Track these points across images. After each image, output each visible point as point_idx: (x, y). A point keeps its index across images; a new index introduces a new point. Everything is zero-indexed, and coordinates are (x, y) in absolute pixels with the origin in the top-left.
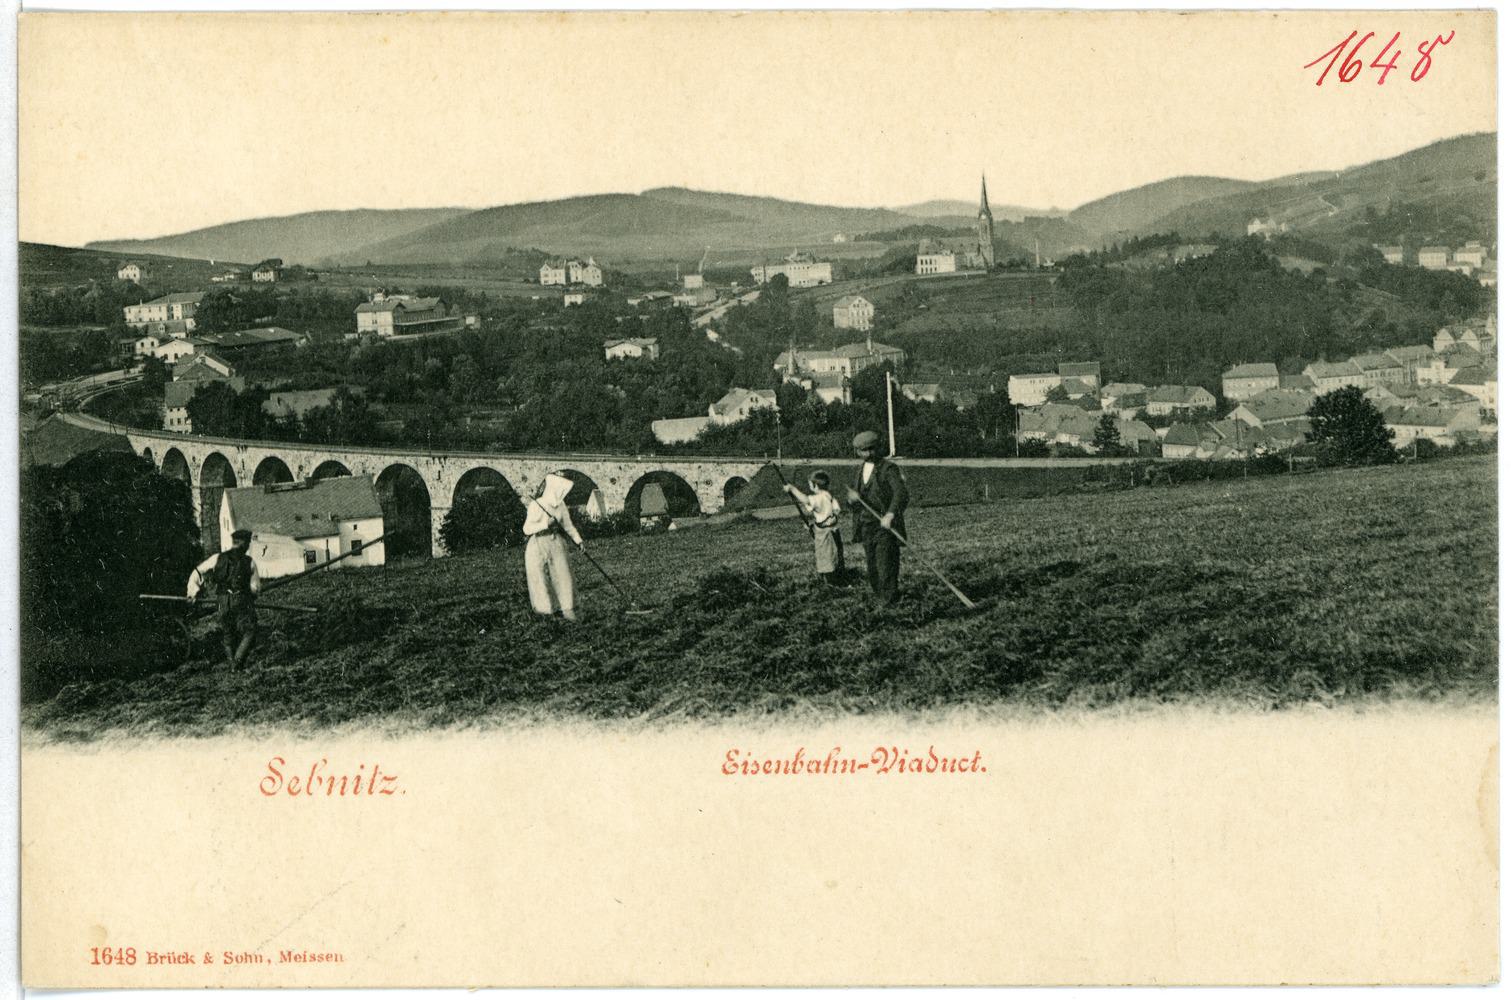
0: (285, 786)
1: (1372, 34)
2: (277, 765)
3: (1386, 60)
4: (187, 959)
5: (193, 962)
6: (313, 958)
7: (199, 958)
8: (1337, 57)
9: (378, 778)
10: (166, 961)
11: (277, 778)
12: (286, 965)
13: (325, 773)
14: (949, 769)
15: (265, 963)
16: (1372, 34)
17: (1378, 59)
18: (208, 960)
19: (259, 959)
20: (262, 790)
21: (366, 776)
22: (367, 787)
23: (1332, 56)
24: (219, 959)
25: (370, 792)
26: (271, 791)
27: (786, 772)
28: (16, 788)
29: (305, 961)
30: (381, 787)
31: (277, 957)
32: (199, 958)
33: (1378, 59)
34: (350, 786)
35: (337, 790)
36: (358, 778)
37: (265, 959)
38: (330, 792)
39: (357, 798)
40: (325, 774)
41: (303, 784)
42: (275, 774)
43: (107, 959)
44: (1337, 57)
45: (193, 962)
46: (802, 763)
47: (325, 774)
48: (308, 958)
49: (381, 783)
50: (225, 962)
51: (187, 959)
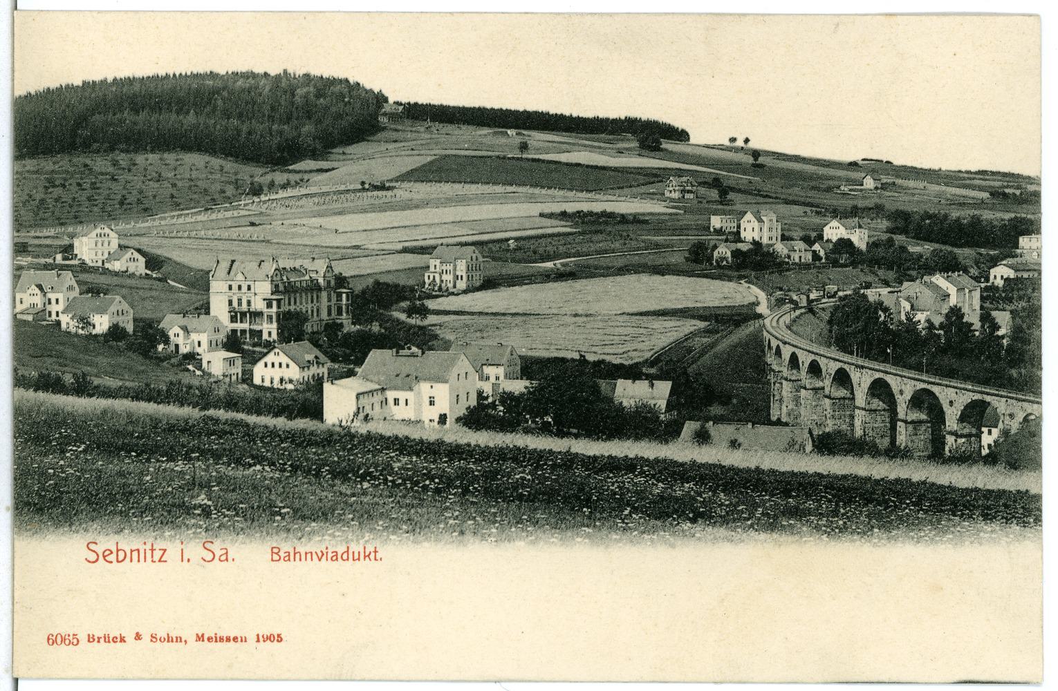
5: (125, 641)
7: (130, 638)
18: (138, 637)
19: (179, 639)
32: (130, 638)
39: (295, 563)
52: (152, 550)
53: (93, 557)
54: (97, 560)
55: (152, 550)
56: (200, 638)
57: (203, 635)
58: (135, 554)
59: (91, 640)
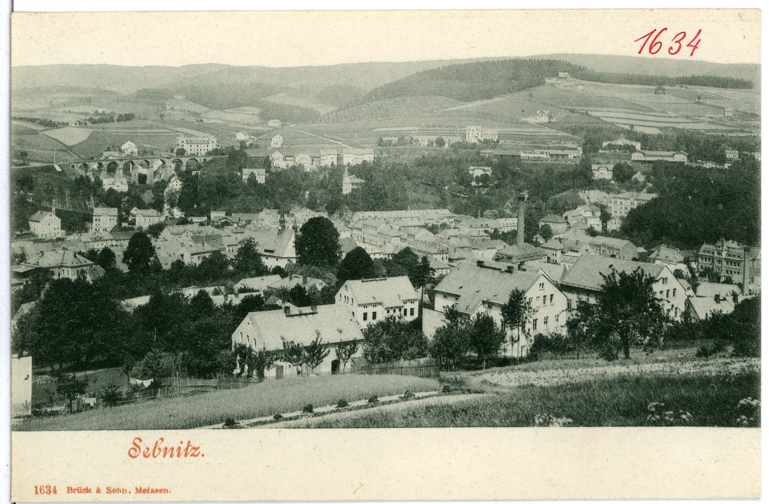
1: (666, 29)
2: (137, 442)
3: (694, 44)
4: (87, 490)
6: (152, 491)
7: (94, 490)
8: (648, 39)
9: (190, 448)
10: (76, 491)
11: (138, 449)
12: (139, 494)
13: (162, 446)
14: (175, 449)
15: (128, 493)
16: (666, 29)
17: (691, 42)
18: (98, 491)
20: (130, 455)
21: (184, 446)
22: (184, 453)
23: (647, 37)
24: (104, 490)
25: (186, 455)
26: (133, 455)
27: (172, 449)
28: (9, 454)
29: (148, 492)
30: (191, 453)
31: (134, 491)
33: (691, 42)
34: (175, 453)
35: (168, 455)
36: (179, 448)
37: (128, 491)
38: (164, 456)
40: (162, 446)
41: (151, 452)
42: (136, 447)
43: (42, 491)
44: (648, 39)
46: (160, 449)
47: (162, 446)
48: (150, 491)
49: (192, 451)
50: (107, 493)
51: (87, 490)
56: (139, 491)
57: (141, 489)
59: (70, 491)
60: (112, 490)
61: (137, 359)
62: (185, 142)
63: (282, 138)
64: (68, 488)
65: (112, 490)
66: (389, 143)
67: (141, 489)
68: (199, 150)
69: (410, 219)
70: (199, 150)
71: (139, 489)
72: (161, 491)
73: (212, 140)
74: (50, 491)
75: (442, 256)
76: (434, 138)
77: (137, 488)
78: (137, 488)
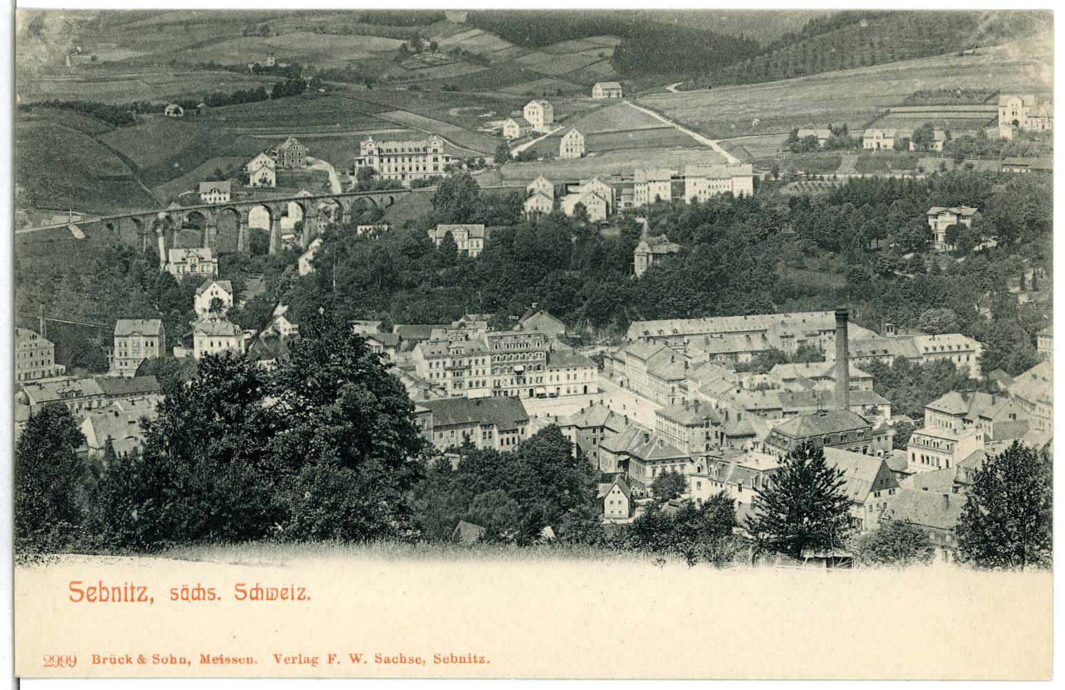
0: (279, 595)
5: (131, 663)
15: (187, 665)
29: (222, 663)
32: (135, 659)
37: (187, 661)
45: (131, 663)
50: (435, 662)
52: (132, 588)
53: (241, 595)
54: (245, 596)
55: (132, 588)
57: (208, 656)
58: (270, 597)
60: (160, 658)
61: (157, 267)
62: (376, 152)
63: (581, 137)
64: (94, 656)
65: (442, 658)
66: (812, 142)
67: (208, 656)
68: (407, 169)
69: (743, 336)
70: (407, 169)
71: (206, 657)
72: (173, 660)
73: (433, 146)
74: (99, 662)
75: (704, 429)
76: (907, 133)
77: (202, 656)
78: (202, 656)
